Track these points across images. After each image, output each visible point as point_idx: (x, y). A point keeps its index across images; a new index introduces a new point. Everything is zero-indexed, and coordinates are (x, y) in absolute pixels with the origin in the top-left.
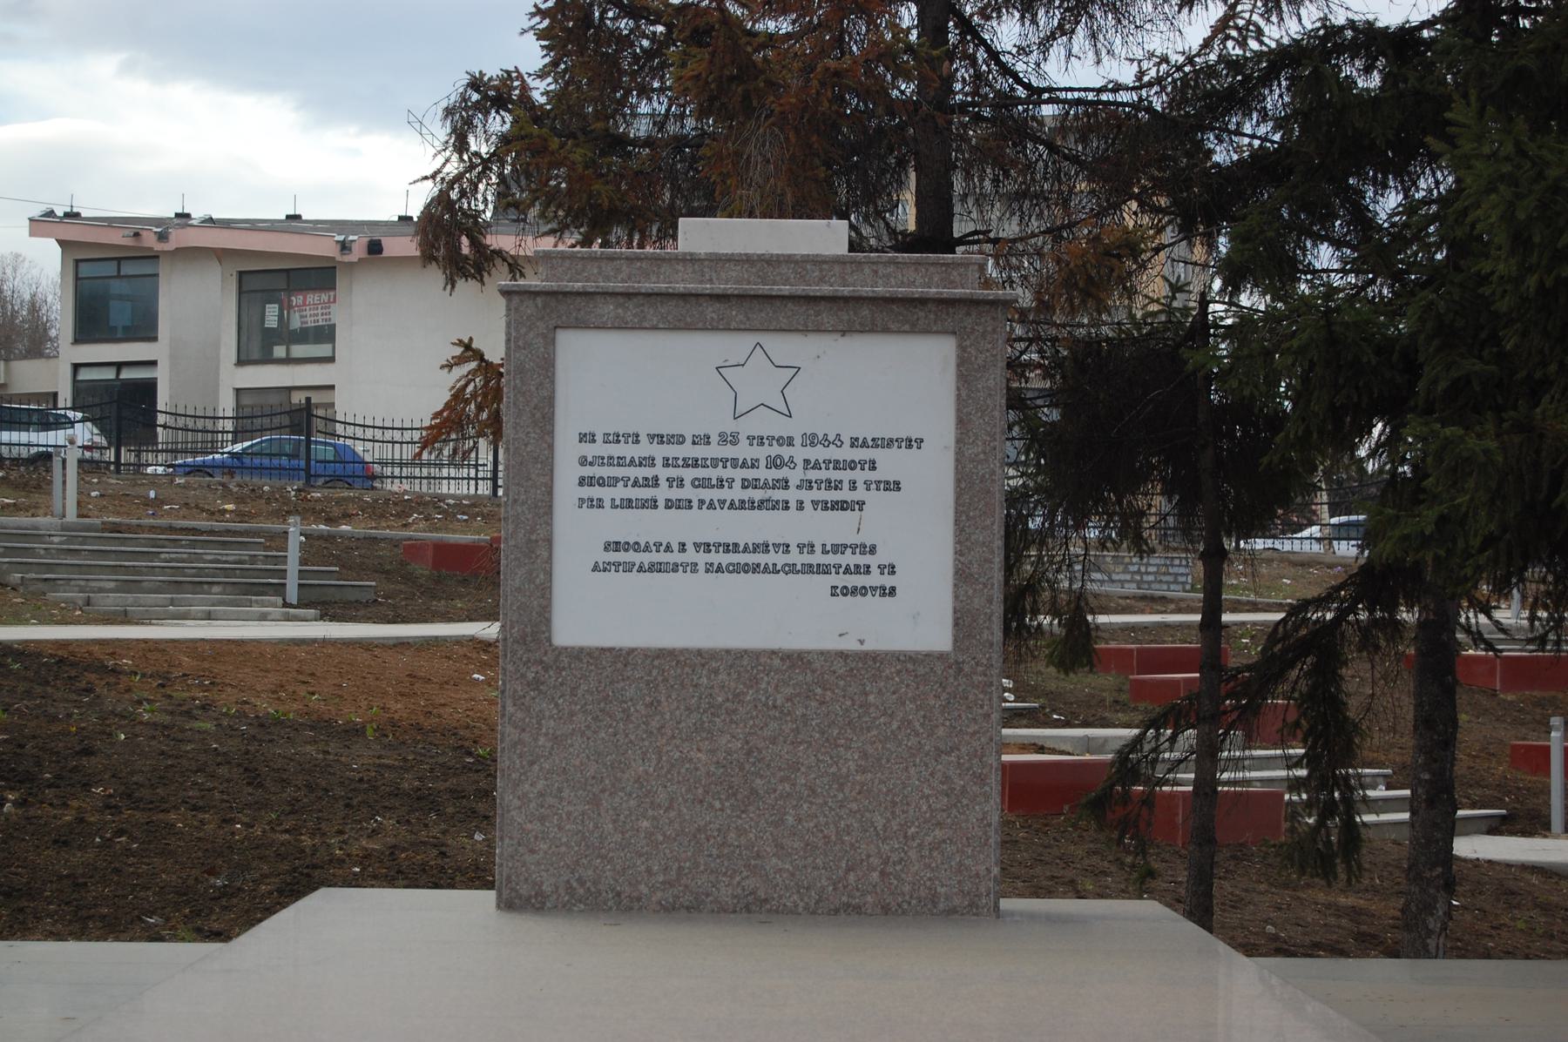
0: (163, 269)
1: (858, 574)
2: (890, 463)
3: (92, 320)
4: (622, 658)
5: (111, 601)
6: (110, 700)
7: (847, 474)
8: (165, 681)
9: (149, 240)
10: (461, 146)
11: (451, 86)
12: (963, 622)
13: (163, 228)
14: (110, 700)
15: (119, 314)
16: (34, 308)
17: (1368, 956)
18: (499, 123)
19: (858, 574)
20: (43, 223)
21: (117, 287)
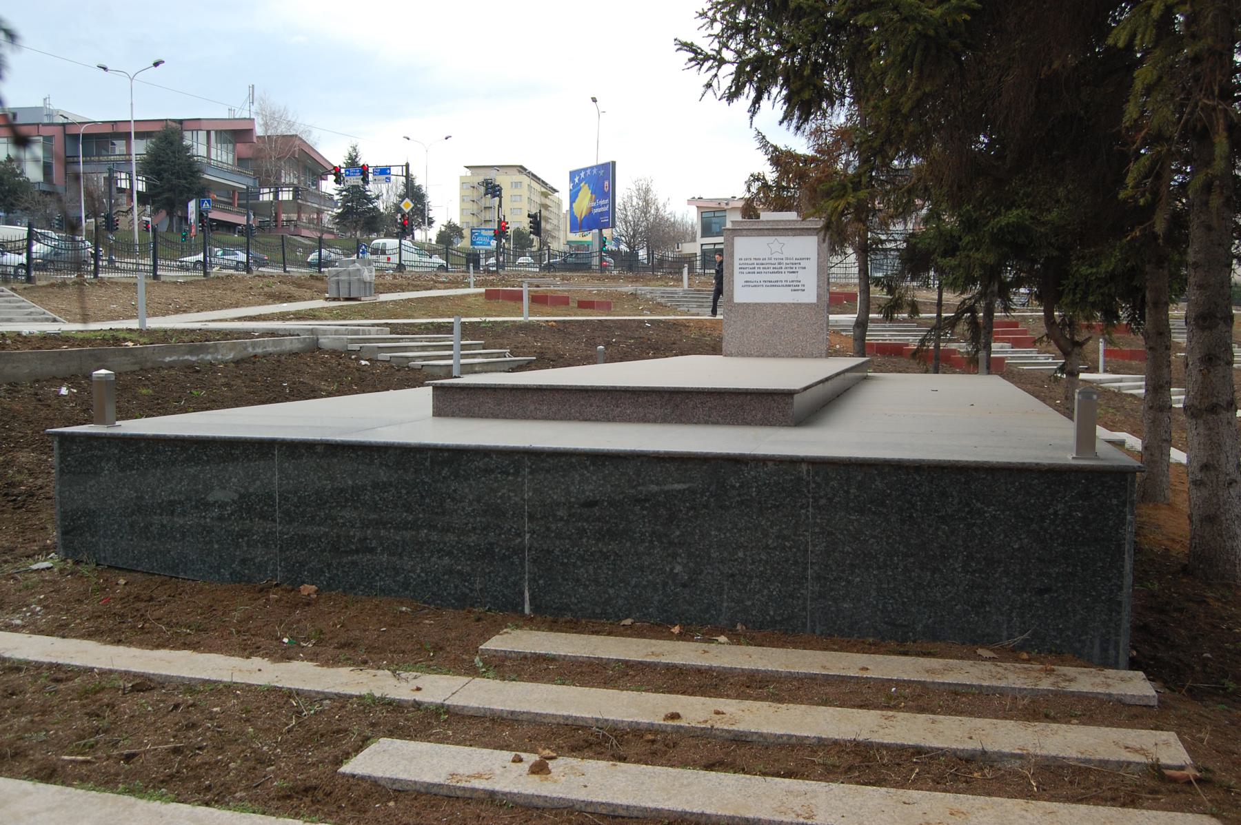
0: (727, 214)
1: (796, 287)
2: (803, 263)
3: (707, 230)
4: (748, 305)
5: (694, 311)
6: (685, 333)
7: (794, 266)
8: (700, 329)
9: (723, 205)
10: (749, 191)
11: (747, 177)
12: (819, 296)
13: (727, 202)
14: (685, 333)
15: (715, 228)
16: (692, 227)
17: (954, 373)
18: (757, 184)
19: (796, 287)
20: (692, 201)
21: (714, 220)
